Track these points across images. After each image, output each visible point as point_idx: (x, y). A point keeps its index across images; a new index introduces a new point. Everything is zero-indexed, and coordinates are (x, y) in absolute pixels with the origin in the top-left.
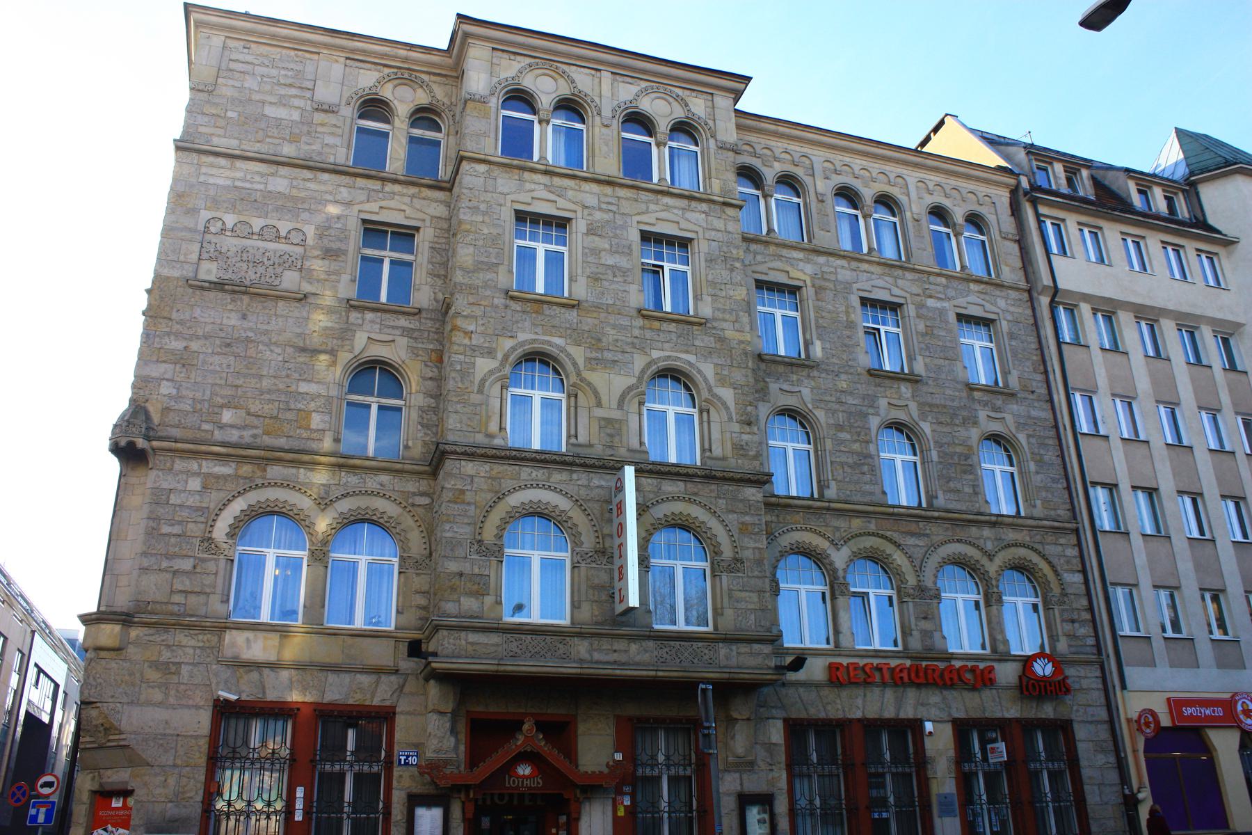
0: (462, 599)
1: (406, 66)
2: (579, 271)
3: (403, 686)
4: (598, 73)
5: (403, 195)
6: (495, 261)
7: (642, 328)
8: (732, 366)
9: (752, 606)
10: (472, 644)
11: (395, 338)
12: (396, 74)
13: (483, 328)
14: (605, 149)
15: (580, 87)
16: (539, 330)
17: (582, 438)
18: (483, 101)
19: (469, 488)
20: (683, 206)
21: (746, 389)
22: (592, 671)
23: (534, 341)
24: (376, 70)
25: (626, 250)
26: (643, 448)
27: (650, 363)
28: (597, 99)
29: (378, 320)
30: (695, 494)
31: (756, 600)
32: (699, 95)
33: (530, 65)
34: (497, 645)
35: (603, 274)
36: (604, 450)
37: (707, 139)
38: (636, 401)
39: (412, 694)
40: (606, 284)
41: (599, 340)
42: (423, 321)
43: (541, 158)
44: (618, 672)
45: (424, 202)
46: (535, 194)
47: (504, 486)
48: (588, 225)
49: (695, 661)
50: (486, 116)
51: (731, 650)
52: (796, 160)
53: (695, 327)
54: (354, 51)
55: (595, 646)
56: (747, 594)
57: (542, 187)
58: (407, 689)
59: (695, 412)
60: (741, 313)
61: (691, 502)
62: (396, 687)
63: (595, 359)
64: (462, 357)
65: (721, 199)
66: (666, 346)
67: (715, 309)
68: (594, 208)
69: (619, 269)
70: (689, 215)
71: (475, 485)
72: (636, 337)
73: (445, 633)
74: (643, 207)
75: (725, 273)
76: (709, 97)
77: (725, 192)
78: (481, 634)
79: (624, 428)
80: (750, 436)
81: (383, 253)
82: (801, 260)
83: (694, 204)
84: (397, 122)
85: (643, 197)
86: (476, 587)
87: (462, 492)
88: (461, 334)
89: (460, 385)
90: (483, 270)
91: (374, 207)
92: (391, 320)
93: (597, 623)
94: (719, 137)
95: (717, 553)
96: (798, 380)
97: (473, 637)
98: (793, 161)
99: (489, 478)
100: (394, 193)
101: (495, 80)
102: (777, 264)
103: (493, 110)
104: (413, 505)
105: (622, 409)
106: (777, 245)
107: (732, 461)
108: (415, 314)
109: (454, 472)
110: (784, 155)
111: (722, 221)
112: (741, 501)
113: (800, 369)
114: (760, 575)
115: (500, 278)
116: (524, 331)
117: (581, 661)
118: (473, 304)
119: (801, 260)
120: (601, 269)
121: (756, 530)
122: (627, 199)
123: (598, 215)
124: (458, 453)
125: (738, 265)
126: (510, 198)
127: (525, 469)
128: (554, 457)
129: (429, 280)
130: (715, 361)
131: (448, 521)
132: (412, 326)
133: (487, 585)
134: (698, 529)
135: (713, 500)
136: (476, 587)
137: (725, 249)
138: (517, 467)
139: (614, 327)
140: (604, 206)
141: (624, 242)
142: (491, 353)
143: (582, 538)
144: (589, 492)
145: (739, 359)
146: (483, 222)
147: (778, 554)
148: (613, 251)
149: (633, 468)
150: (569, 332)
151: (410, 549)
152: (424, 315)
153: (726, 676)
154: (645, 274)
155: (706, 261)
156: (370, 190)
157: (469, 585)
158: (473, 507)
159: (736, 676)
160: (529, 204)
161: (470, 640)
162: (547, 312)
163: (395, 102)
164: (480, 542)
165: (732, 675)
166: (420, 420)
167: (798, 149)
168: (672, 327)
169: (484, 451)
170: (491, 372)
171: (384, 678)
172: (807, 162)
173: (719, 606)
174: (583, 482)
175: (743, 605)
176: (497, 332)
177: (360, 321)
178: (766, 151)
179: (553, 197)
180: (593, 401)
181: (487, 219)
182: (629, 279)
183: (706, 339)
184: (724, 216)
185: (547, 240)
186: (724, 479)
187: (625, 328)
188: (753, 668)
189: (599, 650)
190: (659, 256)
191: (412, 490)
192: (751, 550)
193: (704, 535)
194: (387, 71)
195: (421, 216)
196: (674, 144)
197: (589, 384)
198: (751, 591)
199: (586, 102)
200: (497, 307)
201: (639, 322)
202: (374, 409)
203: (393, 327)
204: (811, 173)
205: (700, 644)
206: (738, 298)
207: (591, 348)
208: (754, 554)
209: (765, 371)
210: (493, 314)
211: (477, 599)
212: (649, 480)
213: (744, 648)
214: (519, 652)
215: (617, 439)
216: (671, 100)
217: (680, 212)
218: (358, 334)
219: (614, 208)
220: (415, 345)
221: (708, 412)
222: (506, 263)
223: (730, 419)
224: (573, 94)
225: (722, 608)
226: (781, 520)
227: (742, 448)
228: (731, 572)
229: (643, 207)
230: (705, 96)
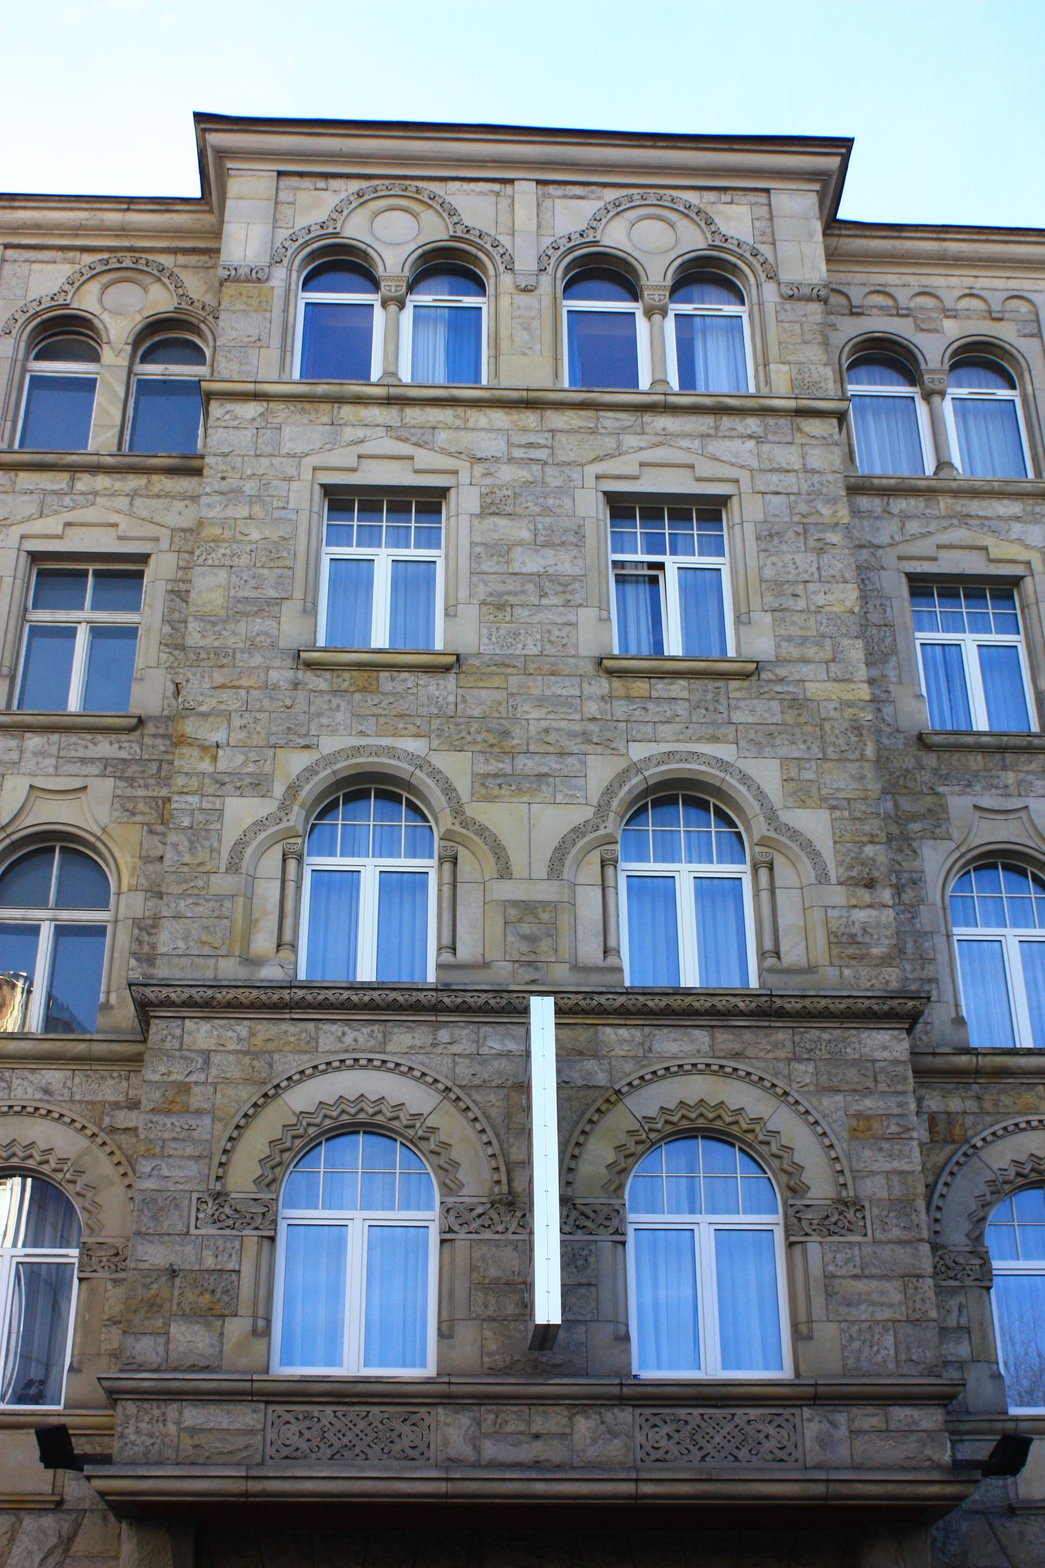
0: (174, 1329)
1: (126, 243)
2: (463, 594)
3: (71, 1539)
4: (509, 189)
5: (114, 494)
6: (272, 593)
7: (608, 698)
8: (825, 759)
9: (886, 1314)
10: (192, 1431)
11: (88, 781)
12: (107, 262)
13: (242, 735)
14: (522, 336)
15: (467, 222)
16: (370, 726)
17: (465, 952)
18: (256, 277)
19: (202, 1077)
20: (704, 429)
21: (860, 806)
22: (474, 1487)
23: (357, 750)
24: (66, 261)
25: (571, 538)
26: (611, 961)
27: (627, 770)
28: (505, 240)
29: (54, 750)
30: (737, 1056)
31: (896, 1297)
32: (738, 197)
33: (359, 195)
34: (250, 1432)
35: (515, 594)
36: (514, 973)
37: (759, 286)
38: (595, 857)
39: (91, 1557)
40: (522, 613)
41: (506, 734)
42: (148, 741)
43: (386, 374)
44: (540, 1488)
45: (155, 503)
46: (366, 449)
47: (278, 1067)
48: (482, 496)
49: (743, 1454)
50: (264, 307)
51: (833, 1424)
52: (996, 306)
53: (734, 684)
54: (17, 229)
55: (487, 1426)
56: (874, 1284)
57: (381, 432)
58: (80, 1545)
59: (742, 870)
60: (846, 642)
61: (727, 1075)
62: (53, 1541)
63: (496, 776)
64: (194, 800)
65: (791, 404)
66: (664, 730)
67: (780, 639)
68: (496, 459)
69: (553, 579)
70: (716, 447)
71: (214, 1072)
72: (593, 719)
73: (131, 1408)
74: (610, 443)
75: (805, 562)
76: (762, 198)
77: (800, 386)
78: (212, 1408)
79: (564, 920)
80: (873, 913)
81: (75, 615)
82: (1017, 518)
83: (726, 422)
84: (107, 355)
85: (608, 423)
86: (207, 1297)
87: (184, 1088)
88: (196, 752)
89: (187, 858)
90: (247, 614)
91: (53, 524)
92: (80, 746)
93: (493, 1371)
94: (783, 277)
95: (795, 1189)
96: (1019, 783)
97: (193, 1415)
98: (990, 312)
99: (247, 1053)
100: (95, 494)
101: (283, 234)
102: (960, 535)
103: (279, 293)
104: (113, 1130)
105: (558, 878)
106: (956, 493)
107: (831, 974)
108: (131, 730)
109: (168, 1045)
110: (965, 303)
111: (793, 449)
112: (855, 1063)
113: (1023, 758)
114: (906, 1235)
115: (285, 626)
116: (333, 731)
117: (453, 1462)
118: (222, 687)
119: (1017, 518)
120: (513, 585)
121: (894, 1129)
122: (571, 431)
123: (506, 473)
124: (173, 1004)
125: (834, 538)
126: (309, 462)
127: (327, 1027)
128: (393, 995)
129: (164, 656)
130: (785, 751)
131: (150, 1155)
132: (124, 754)
133: (232, 1293)
134: (750, 1137)
135: (781, 1065)
136: (207, 1297)
137: (803, 508)
138: (311, 1026)
139: (540, 702)
140: (518, 453)
141: (566, 523)
142: (259, 785)
143: (462, 1175)
144: (478, 1068)
145: (841, 741)
146: (250, 518)
147: (985, 1189)
148: (538, 544)
149: (550, 1001)
150: (436, 723)
151: (102, 1226)
152: (150, 728)
153: (819, 1489)
154: (630, 589)
155: (758, 538)
156: (45, 492)
157: (191, 1296)
158: (207, 1120)
159: (845, 1489)
160: (354, 470)
161: (188, 1423)
162: (388, 687)
163: (105, 317)
164: (219, 1197)
165: (833, 1488)
166: (135, 947)
167: (1000, 284)
168: (679, 688)
169: (232, 993)
170: (259, 825)
171: (29, 1522)
172: (1024, 308)
173: (802, 1317)
174: (464, 1046)
175: (863, 1312)
176: (273, 740)
177: (15, 756)
178: (922, 300)
179: (405, 449)
180: (490, 866)
181: (257, 509)
182: (577, 599)
183: (760, 705)
184: (799, 439)
185: (400, 540)
186: (805, 1016)
187: (564, 702)
188: (892, 1468)
189: (497, 1435)
190: (654, 545)
191: (113, 1098)
192: (880, 1180)
193: (764, 1149)
194: (87, 259)
195: (151, 530)
196: (686, 308)
197: (482, 831)
198: (884, 1277)
199: (481, 248)
200: (276, 687)
201: (602, 685)
202: (46, 933)
203: (83, 761)
204: (1032, 328)
205: (753, 1413)
206: (838, 609)
207: (488, 751)
208: (890, 1187)
209: (935, 771)
210: (266, 703)
211: (208, 1325)
212: (623, 1032)
213: (868, 1419)
214: (304, 1446)
215: (544, 946)
216: (673, 216)
217: (696, 444)
218: (10, 782)
219: (541, 454)
220: (129, 792)
221: (771, 868)
222: (298, 594)
223: (823, 878)
224: (454, 238)
225: (810, 1322)
226: (988, 1106)
227: (852, 938)
228: (831, 1234)
229: (610, 443)
230: (753, 197)
